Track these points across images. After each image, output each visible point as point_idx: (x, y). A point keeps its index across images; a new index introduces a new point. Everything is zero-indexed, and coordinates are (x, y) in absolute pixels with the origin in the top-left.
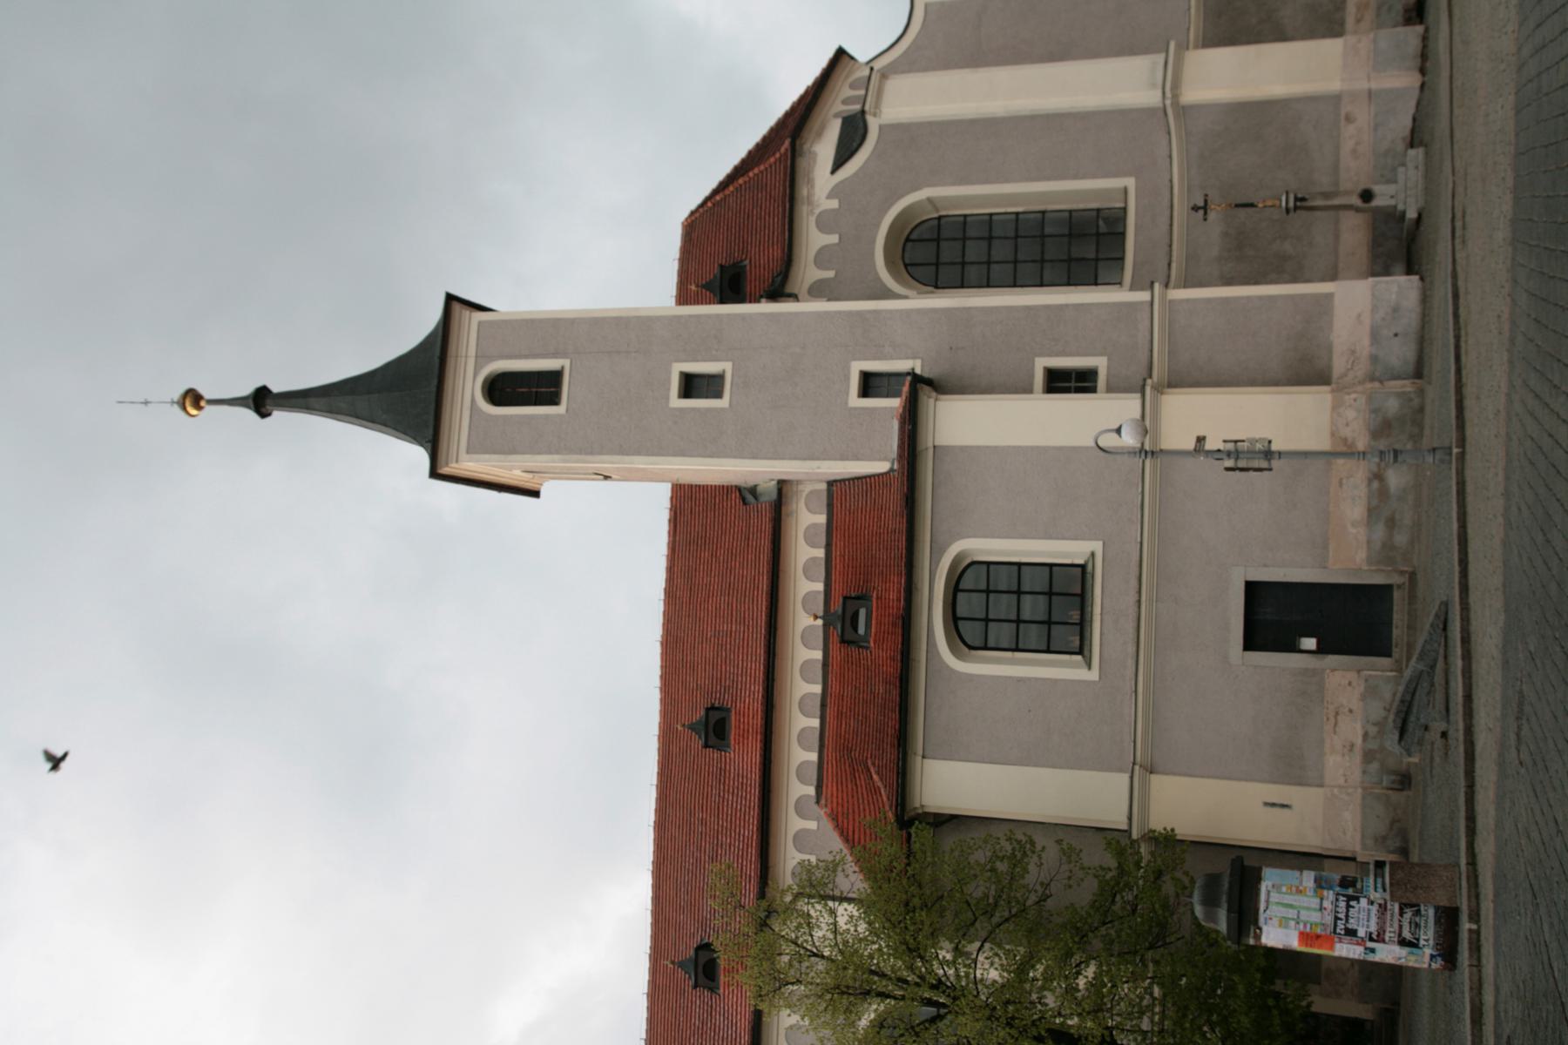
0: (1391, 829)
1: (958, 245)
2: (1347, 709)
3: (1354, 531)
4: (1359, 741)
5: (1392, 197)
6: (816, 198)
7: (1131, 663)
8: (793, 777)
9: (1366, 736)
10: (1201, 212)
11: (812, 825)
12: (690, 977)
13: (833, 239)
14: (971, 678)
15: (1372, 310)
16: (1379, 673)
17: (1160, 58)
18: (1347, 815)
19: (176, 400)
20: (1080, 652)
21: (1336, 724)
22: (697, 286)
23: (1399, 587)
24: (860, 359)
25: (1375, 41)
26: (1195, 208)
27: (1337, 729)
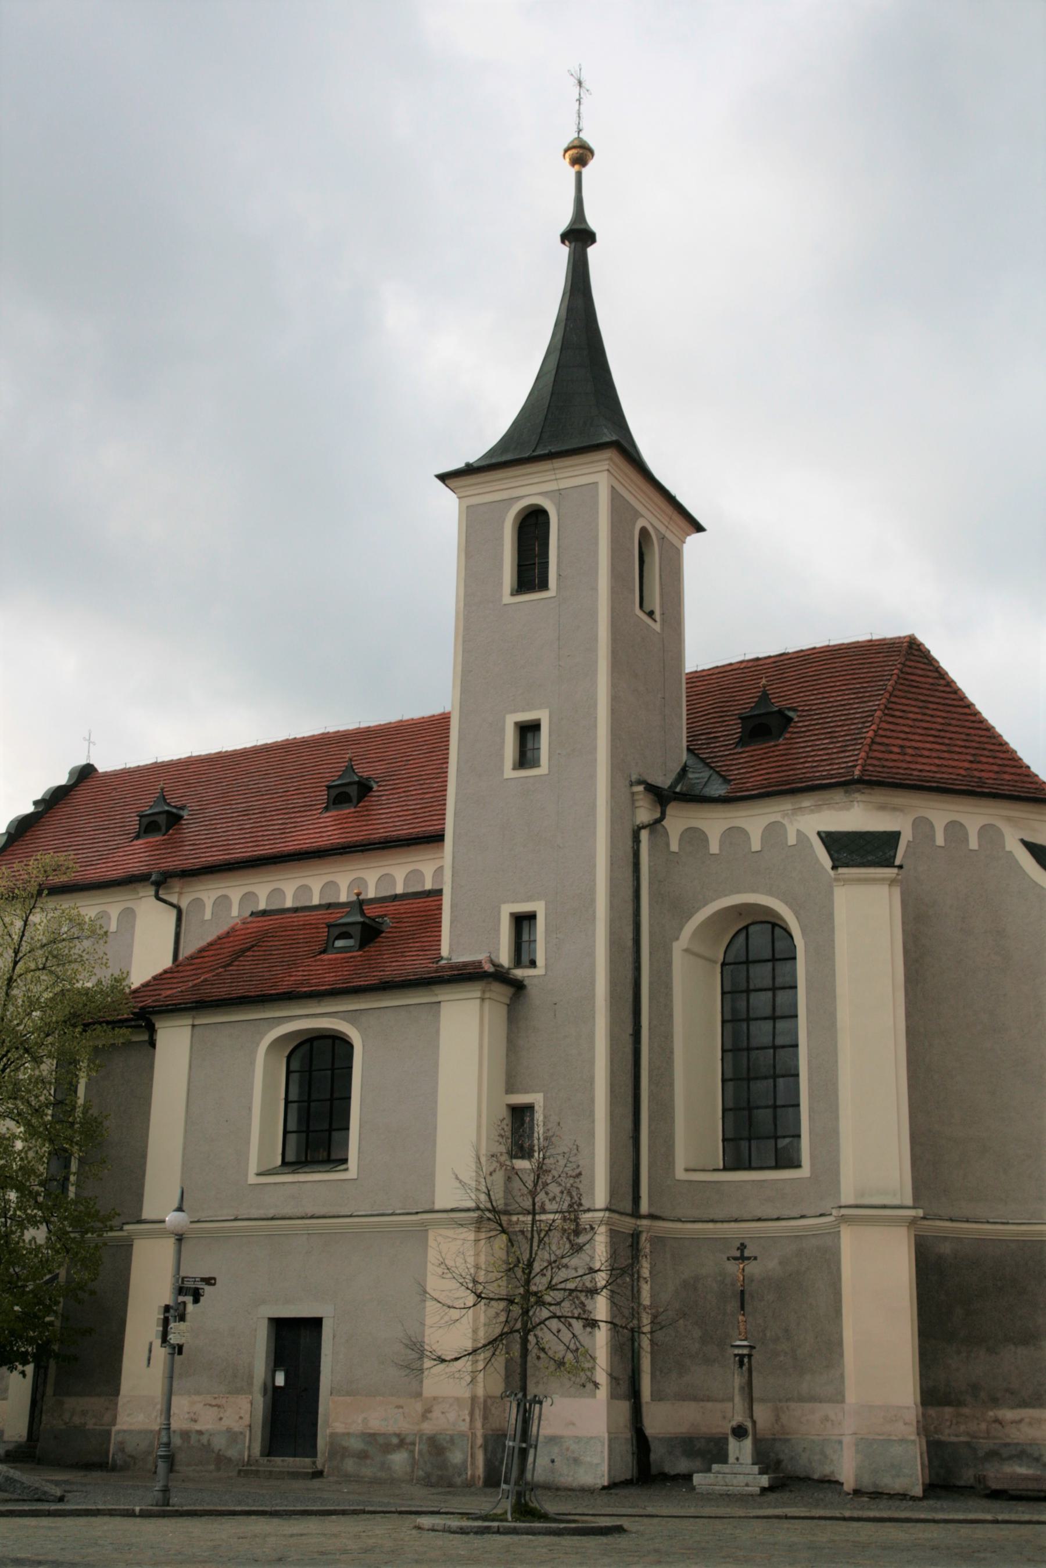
0: (129, 1456)
1: (768, 984)
2: (222, 1415)
3: (360, 1421)
4: (197, 1427)
5: (737, 1459)
6: (798, 818)
7: (255, 1213)
8: (220, 893)
9: (200, 1433)
10: (738, 1254)
11: (235, 912)
12: (151, 807)
13: (756, 845)
14: (253, 1063)
15: (577, 1437)
16: (247, 1444)
17: (909, 1201)
18: (141, 1417)
19: (582, 135)
20: (284, 1163)
21: (210, 1405)
22: (764, 686)
23: (314, 1463)
24: (546, 909)
25: (902, 1441)
26: (742, 1247)
27: (208, 1407)
